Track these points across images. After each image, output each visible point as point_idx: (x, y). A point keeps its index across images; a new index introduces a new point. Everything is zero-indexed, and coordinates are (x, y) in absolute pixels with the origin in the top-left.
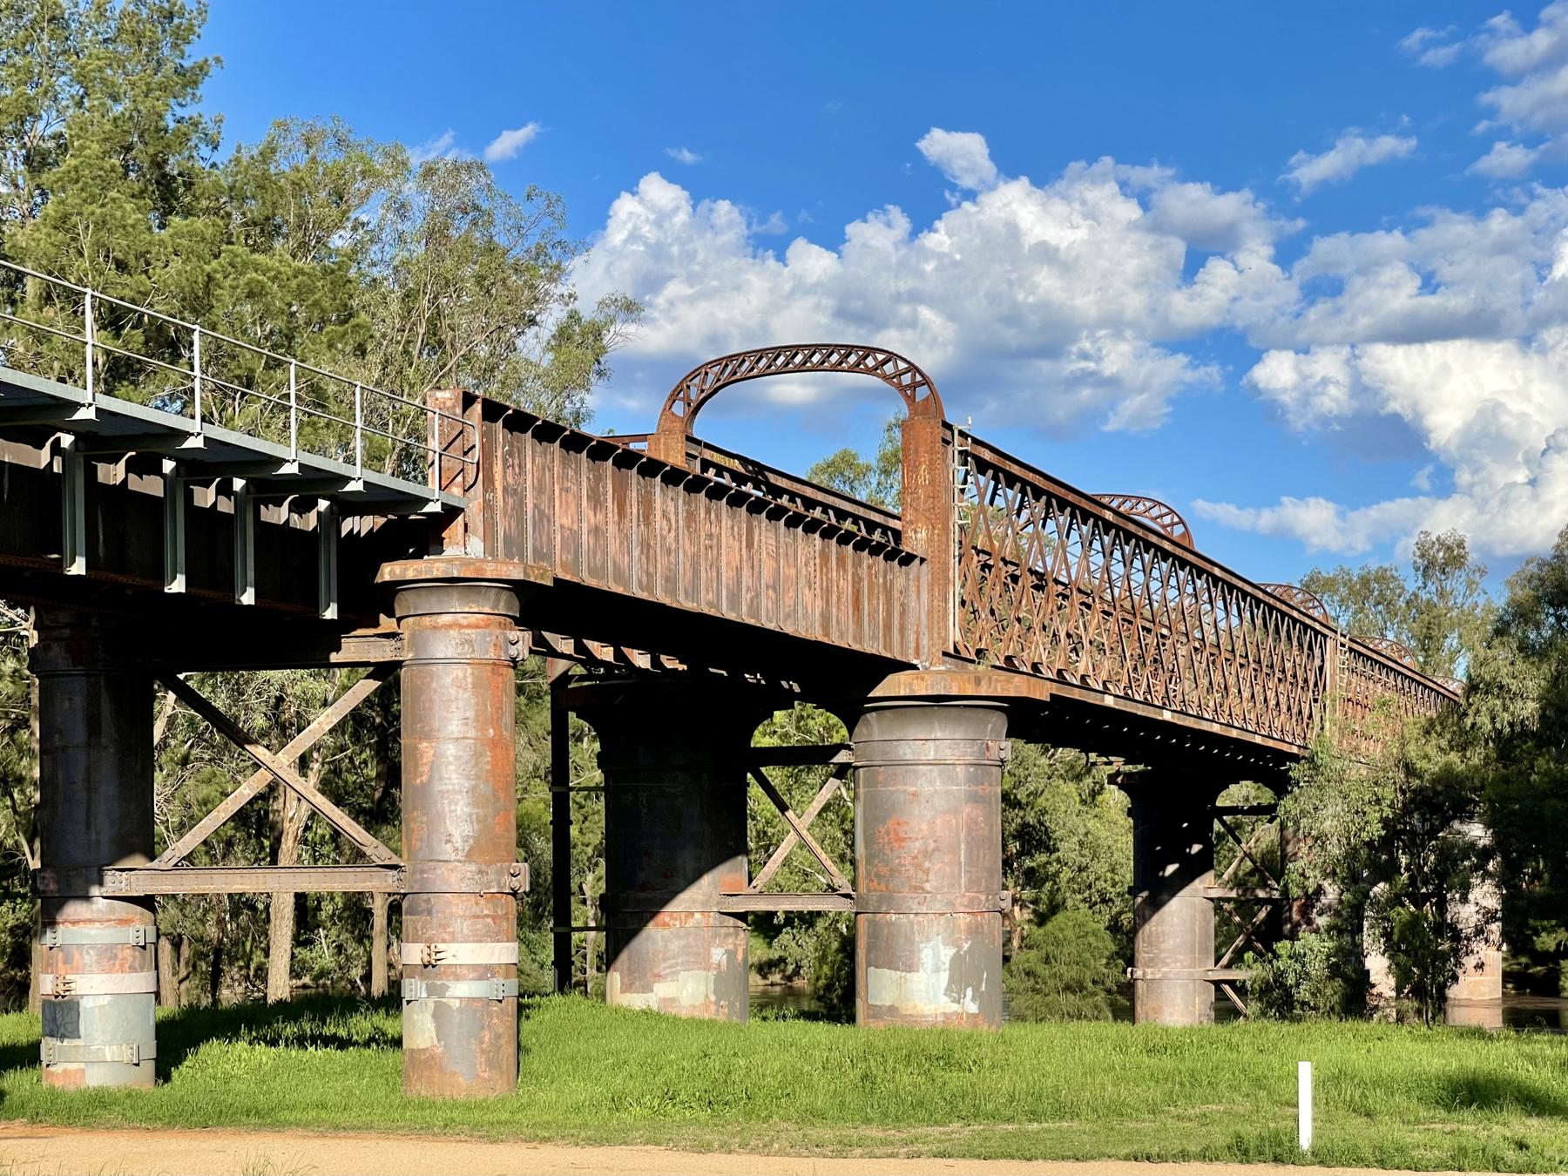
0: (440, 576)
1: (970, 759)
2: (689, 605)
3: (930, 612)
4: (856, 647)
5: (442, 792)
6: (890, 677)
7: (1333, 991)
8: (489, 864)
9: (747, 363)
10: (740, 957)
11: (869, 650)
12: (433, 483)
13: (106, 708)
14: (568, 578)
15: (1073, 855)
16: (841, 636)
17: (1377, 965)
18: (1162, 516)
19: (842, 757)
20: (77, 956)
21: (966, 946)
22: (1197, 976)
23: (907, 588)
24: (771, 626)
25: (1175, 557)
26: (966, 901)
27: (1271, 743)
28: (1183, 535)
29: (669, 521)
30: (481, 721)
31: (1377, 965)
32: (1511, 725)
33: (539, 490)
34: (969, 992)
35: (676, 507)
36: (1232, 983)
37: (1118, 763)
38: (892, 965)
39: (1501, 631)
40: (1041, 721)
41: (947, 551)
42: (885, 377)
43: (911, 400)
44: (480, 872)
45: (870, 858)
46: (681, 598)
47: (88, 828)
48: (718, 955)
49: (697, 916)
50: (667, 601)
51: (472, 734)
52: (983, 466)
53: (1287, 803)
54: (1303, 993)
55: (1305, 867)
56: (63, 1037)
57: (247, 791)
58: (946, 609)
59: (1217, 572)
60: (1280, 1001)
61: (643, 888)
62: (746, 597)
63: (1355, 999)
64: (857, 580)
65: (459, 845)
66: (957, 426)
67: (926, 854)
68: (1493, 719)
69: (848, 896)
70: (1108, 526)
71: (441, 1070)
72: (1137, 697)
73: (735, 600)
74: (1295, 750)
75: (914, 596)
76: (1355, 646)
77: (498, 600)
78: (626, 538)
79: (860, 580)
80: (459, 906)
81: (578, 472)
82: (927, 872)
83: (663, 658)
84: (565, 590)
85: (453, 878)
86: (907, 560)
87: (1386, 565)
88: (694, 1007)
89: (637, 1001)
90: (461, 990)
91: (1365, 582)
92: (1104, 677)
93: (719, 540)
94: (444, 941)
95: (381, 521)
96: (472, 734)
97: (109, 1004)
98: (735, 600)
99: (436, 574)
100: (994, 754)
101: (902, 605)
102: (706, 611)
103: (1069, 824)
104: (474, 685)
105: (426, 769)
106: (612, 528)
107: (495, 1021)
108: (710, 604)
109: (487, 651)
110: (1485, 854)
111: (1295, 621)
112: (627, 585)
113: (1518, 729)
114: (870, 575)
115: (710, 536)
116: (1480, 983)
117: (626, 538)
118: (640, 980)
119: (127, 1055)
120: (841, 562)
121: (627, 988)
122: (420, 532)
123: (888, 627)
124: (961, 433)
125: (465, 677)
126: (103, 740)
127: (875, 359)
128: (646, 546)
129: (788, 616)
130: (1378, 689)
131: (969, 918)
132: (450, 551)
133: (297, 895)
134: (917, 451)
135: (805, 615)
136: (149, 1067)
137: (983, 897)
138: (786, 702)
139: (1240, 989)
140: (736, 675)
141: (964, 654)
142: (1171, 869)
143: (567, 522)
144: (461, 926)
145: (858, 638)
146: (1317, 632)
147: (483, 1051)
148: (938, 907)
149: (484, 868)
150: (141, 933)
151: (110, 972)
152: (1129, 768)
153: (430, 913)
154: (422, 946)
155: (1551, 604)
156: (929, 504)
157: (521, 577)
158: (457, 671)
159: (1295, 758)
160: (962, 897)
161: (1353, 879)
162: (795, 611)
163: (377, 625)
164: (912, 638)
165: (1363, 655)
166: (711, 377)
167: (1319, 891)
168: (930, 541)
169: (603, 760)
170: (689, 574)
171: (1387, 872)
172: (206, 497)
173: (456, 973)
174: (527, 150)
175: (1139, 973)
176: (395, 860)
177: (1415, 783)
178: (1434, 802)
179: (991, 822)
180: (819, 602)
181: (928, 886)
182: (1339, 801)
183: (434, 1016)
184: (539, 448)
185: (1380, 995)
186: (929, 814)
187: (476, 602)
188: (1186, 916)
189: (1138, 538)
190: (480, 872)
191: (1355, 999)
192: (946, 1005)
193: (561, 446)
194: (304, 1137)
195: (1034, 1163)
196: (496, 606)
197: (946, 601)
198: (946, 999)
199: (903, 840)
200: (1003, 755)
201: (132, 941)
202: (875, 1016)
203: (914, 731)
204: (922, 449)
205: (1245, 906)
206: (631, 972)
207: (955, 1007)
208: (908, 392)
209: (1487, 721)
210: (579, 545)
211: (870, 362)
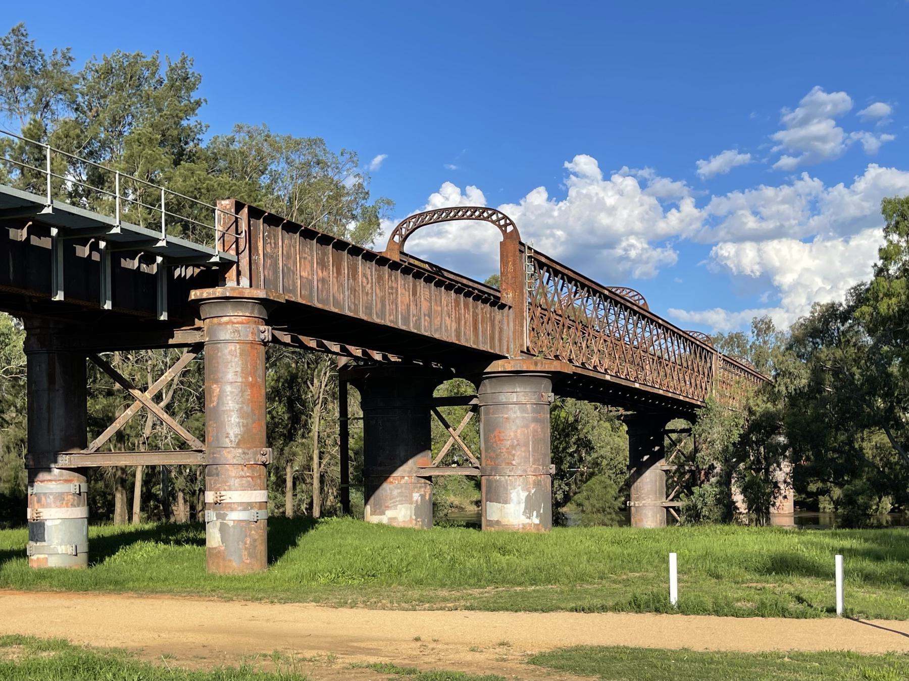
1: (534, 401)
3: (514, 332)
4: (474, 346)
7: (717, 512)
8: (249, 449)
10: (427, 498)
13: (58, 370)
14: (304, 302)
16: (467, 341)
17: (738, 498)
19: (474, 401)
20: (43, 499)
21: (533, 491)
24: (426, 334)
25: (640, 314)
27: (687, 400)
30: (245, 373)
31: (738, 498)
32: (795, 390)
33: (288, 257)
34: (535, 513)
35: (371, 272)
36: (673, 508)
37: (621, 411)
39: (790, 348)
40: (567, 385)
41: (522, 303)
42: (493, 222)
43: (504, 232)
44: (244, 453)
45: (487, 449)
46: (375, 317)
47: (49, 432)
48: (416, 496)
50: (365, 318)
51: (240, 380)
52: (541, 265)
53: (696, 428)
54: (705, 512)
55: (706, 456)
56: (37, 541)
57: (130, 413)
58: (522, 330)
59: (660, 321)
60: (694, 516)
62: (413, 320)
63: (728, 514)
64: (475, 316)
65: (233, 439)
67: (513, 447)
70: (606, 298)
71: (224, 559)
73: (406, 320)
74: (699, 403)
75: (506, 323)
78: (341, 285)
79: (477, 315)
80: (233, 472)
81: (311, 249)
82: (514, 455)
83: (390, 356)
84: (291, 305)
85: (229, 456)
86: (502, 307)
89: (375, 519)
90: (234, 516)
91: (731, 338)
92: (608, 368)
93: (397, 291)
94: (225, 490)
95: (197, 271)
96: (240, 380)
97: (60, 524)
98: (406, 320)
99: (218, 295)
102: (389, 324)
104: (241, 354)
106: (332, 280)
108: (391, 321)
110: (785, 448)
111: (698, 346)
112: (343, 308)
113: (798, 391)
115: (392, 288)
116: (784, 506)
118: (379, 510)
119: (70, 550)
120: (466, 306)
121: (373, 513)
122: (214, 275)
124: (530, 248)
126: (57, 387)
128: (353, 290)
129: (436, 330)
130: (735, 377)
131: (534, 478)
132: (231, 283)
135: (446, 330)
136: (83, 557)
138: (450, 376)
139: (677, 510)
140: (427, 364)
142: (646, 458)
143: (304, 274)
146: (708, 351)
147: (246, 549)
148: (519, 472)
149: (246, 451)
150: (78, 487)
151: (60, 507)
152: (624, 413)
153: (218, 475)
154: (213, 492)
155: (810, 336)
157: (264, 296)
158: (232, 347)
159: (699, 407)
161: (727, 461)
163: (194, 324)
164: (505, 344)
165: (728, 362)
166: (412, 224)
167: (712, 467)
168: (514, 298)
169: (363, 405)
170: (379, 306)
171: (743, 457)
172: (83, 251)
173: (231, 507)
174: (384, 162)
175: (632, 504)
177: (753, 418)
178: (761, 427)
180: (454, 324)
181: (514, 462)
183: (220, 530)
184: (286, 235)
185: (740, 513)
186: (514, 428)
188: (652, 480)
189: (621, 304)
191: (728, 514)
192: (523, 520)
193: (283, 229)
195: (519, 613)
197: (523, 327)
200: (550, 399)
201: (73, 491)
205: (680, 472)
206: (375, 505)
207: (528, 521)
208: (503, 228)
209: (784, 389)
211: (485, 215)
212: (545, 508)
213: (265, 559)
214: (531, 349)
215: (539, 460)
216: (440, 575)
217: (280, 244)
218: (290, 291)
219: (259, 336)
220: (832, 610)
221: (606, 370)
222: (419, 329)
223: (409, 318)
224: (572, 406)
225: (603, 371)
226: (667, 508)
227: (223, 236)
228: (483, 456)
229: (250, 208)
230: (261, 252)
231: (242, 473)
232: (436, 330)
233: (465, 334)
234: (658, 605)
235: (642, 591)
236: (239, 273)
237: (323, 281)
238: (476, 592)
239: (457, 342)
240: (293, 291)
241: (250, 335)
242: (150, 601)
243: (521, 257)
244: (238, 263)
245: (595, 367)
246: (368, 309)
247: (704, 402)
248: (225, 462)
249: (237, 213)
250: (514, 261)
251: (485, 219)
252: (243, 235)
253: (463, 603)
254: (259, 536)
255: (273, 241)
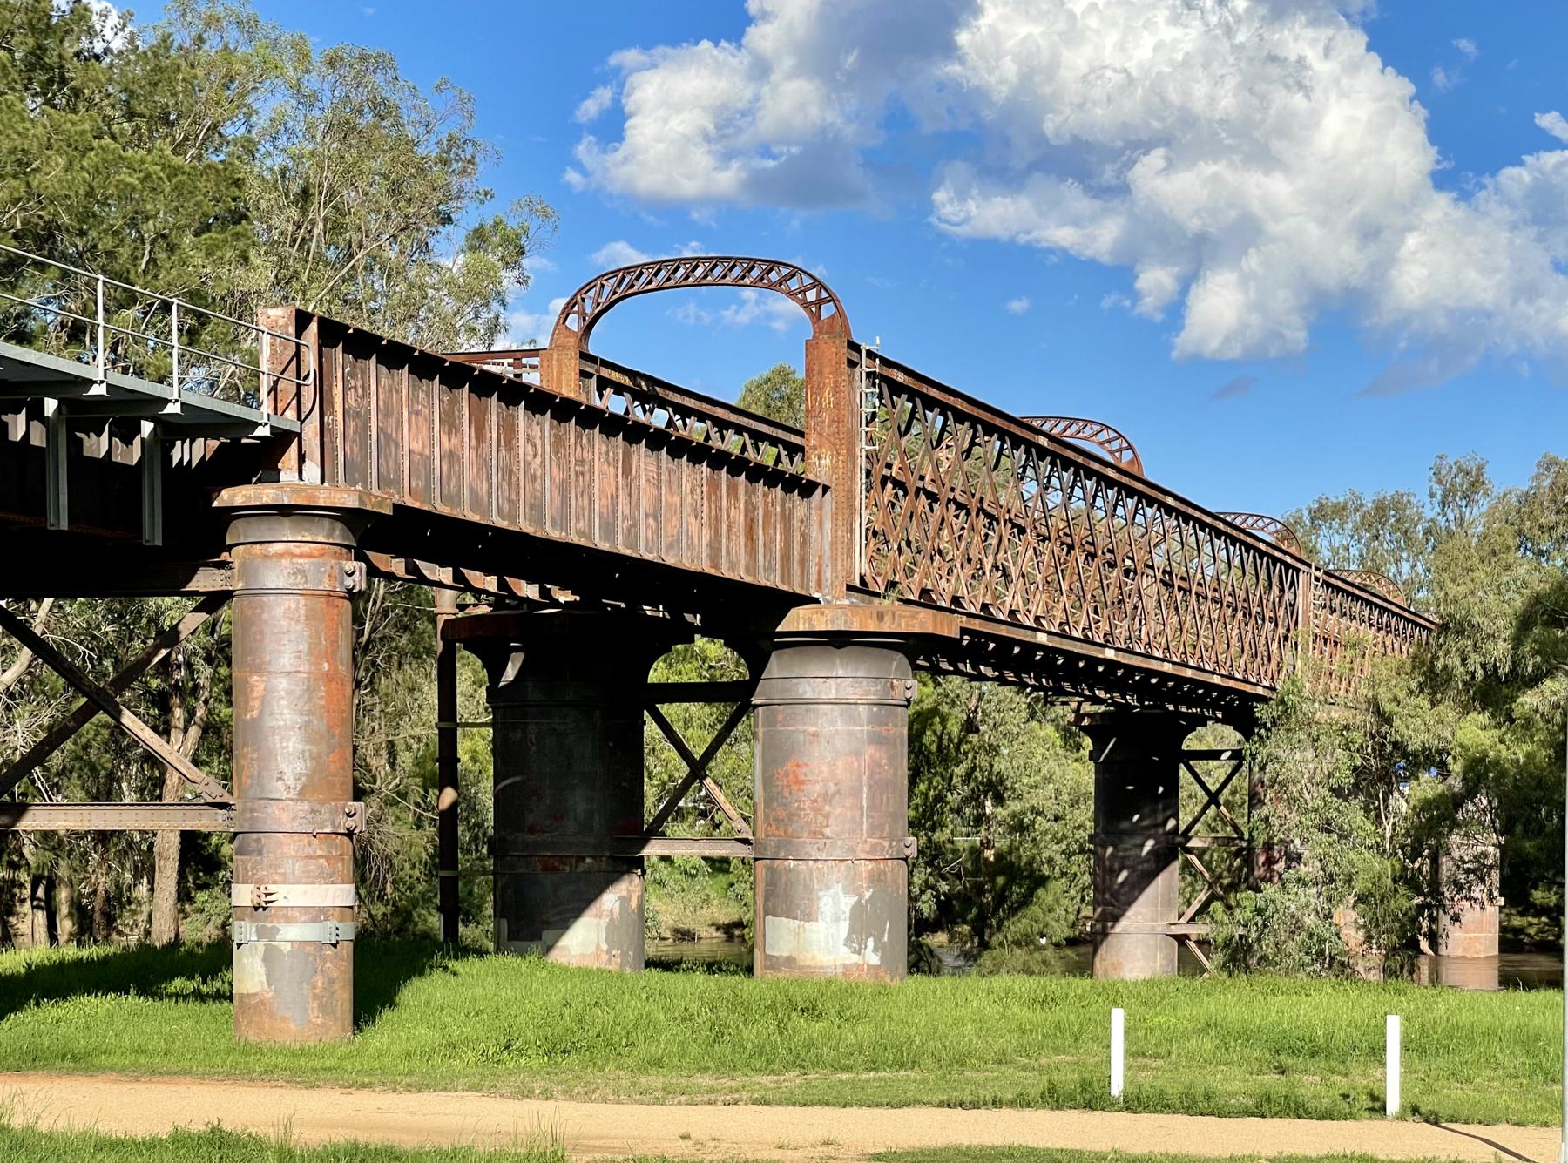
0: (270, 502)
1: (874, 698)
2: (555, 534)
3: (833, 544)
4: (748, 579)
5: (273, 729)
6: (794, 611)
8: (322, 803)
9: (663, 273)
10: (634, 903)
11: (764, 582)
12: (267, 408)
14: (417, 505)
15: (1049, 803)
16: (732, 568)
18: (1109, 441)
21: (868, 895)
22: (1159, 930)
23: (809, 517)
24: (650, 557)
26: (868, 848)
27: (1232, 684)
28: (1131, 462)
29: (534, 446)
30: (315, 654)
33: (386, 413)
34: (871, 943)
35: (543, 431)
38: (790, 915)
41: (852, 479)
44: (313, 811)
45: (768, 802)
49: (588, 860)
50: (530, 530)
51: (305, 667)
52: (896, 389)
58: (851, 539)
61: (532, 830)
62: (622, 526)
64: (750, 510)
65: (291, 783)
66: (865, 347)
67: (827, 798)
68: (1464, 660)
69: (745, 841)
70: (1042, 453)
71: (272, 1015)
72: (1075, 634)
73: (609, 529)
74: (1260, 691)
76: (1333, 581)
77: (332, 531)
78: (484, 463)
79: (755, 508)
80: (289, 847)
81: (429, 394)
82: (827, 816)
85: (285, 817)
86: (807, 489)
87: (1402, 491)
88: (583, 955)
90: (291, 933)
91: (1381, 507)
93: (592, 467)
94: (275, 883)
95: (214, 444)
98: (609, 529)
99: (265, 501)
100: (900, 694)
101: (803, 535)
102: (576, 540)
103: (1044, 770)
105: (257, 703)
107: (328, 965)
108: (580, 533)
109: (321, 582)
114: (766, 503)
115: (582, 462)
117: (484, 463)
120: (732, 491)
122: (259, 458)
123: (786, 559)
124: (870, 354)
125: (297, 609)
127: (779, 272)
128: (508, 472)
129: (670, 547)
131: (871, 865)
132: (288, 475)
133: (184, 834)
134: (821, 373)
135: (691, 546)
137: (886, 844)
141: (873, 587)
143: (416, 446)
144: (294, 867)
145: (751, 569)
146: (1288, 566)
147: (315, 996)
148: (838, 854)
149: (317, 807)
153: (260, 853)
154: (252, 886)
156: (833, 429)
157: (356, 505)
158: (289, 603)
159: (1264, 700)
160: (863, 843)
162: (679, 540)
164: (814, 570)
166: (607, 289)
168: (834, 467)
170: (557, 502)
173: (287, 915)
176: (227, 799)
179: (245, 759)
180: (705, 530)
181: (827, 831)
182: (1308, 745)
183: (265, 960)
187: (308, 530)
190: (313, 811)
194: (116, 1082)
196: (330, 535)
197: (852, 531)
198: (846, 950)
199: (803, 782)
202: (772, 967)
203: (815, 669)
204: (826, 370)
207: (855, 958)
209: (1458, 662)
210: (430, 471)
211: (774, 276)
212: (895, 930)
213: (349, 1017)
214: (868, 579)
215: (881, 827)
216: (695, 1050)
217: (373, 387)
218: (390, 483)
219: (342, 583)
220: (1377, 1107)
221: (1037, 619)
222: (634, 547)
223: (614, 525)
224: (959, 691)
225: (1031, 623)
226: (1181, 939)
227: (276, 383)
228: (760, 814)
229: (321, 321)
230: (338, 407)
231: (309, 851)
232: (670, 547)
233: (728, 553)
234: (1092, 1098)
235: (1069, 1079)
236: (302, 458)
237: (451, 457)
238: (766, 1080)
239: (713, 572)
240: (396, 483)
241: (326, 580)
242: (163, 1087)
243: (851, 377)
244: (299, 435)
245: (1012, 613)
246: (536, 509)
247: (1273, 689)
248: (274, 828)
249: (299, 336)
250: (836, 385)
251: (772, 286)
252: (311, 380)
253: (745, 1095)
254: (339, 969)
255: (359, 383)
